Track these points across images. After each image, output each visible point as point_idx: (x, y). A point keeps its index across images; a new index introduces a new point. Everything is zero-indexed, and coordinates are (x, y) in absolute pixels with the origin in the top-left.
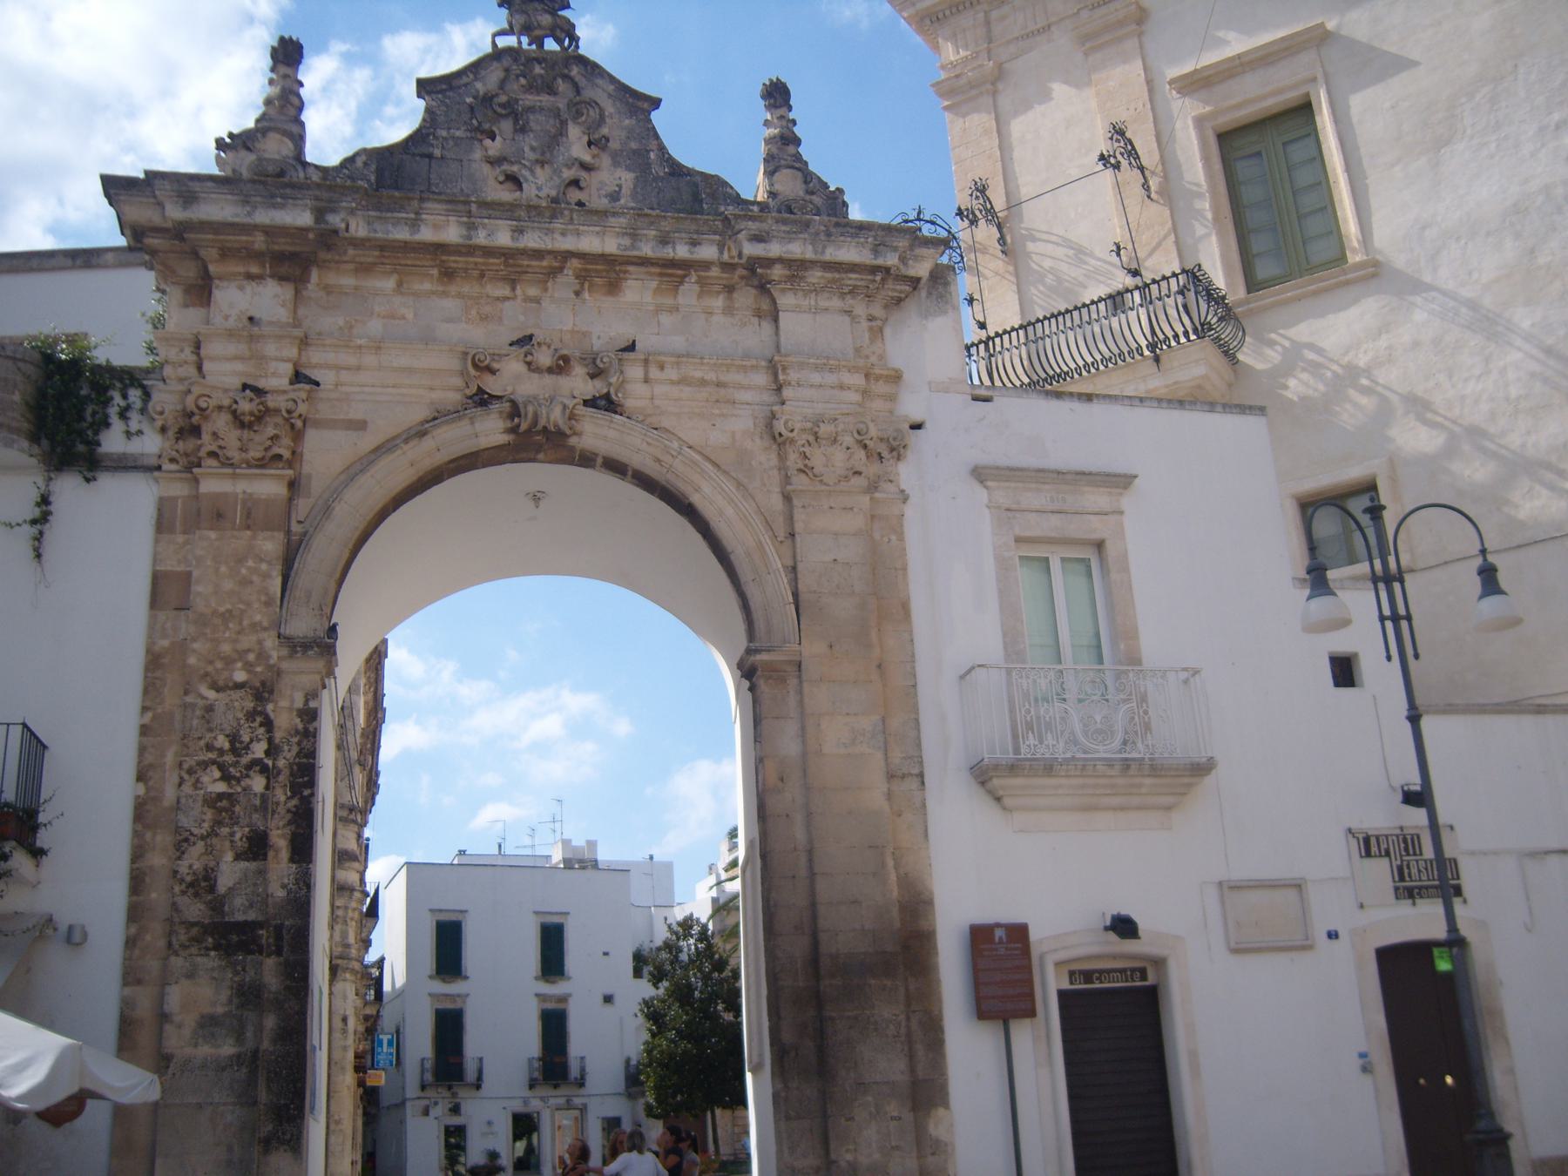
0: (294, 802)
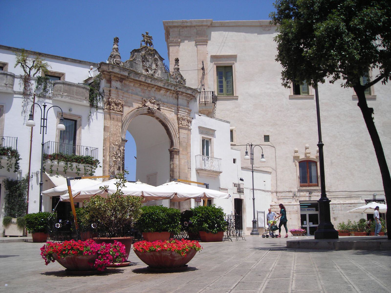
0: (122, 163)
